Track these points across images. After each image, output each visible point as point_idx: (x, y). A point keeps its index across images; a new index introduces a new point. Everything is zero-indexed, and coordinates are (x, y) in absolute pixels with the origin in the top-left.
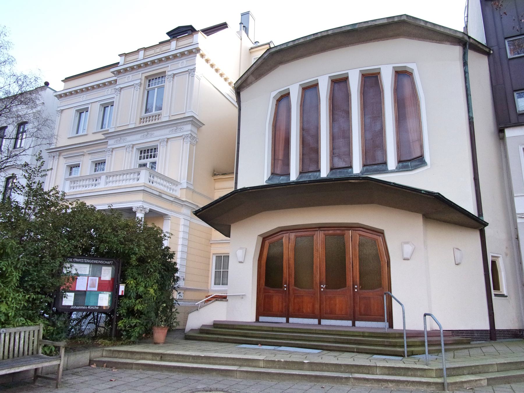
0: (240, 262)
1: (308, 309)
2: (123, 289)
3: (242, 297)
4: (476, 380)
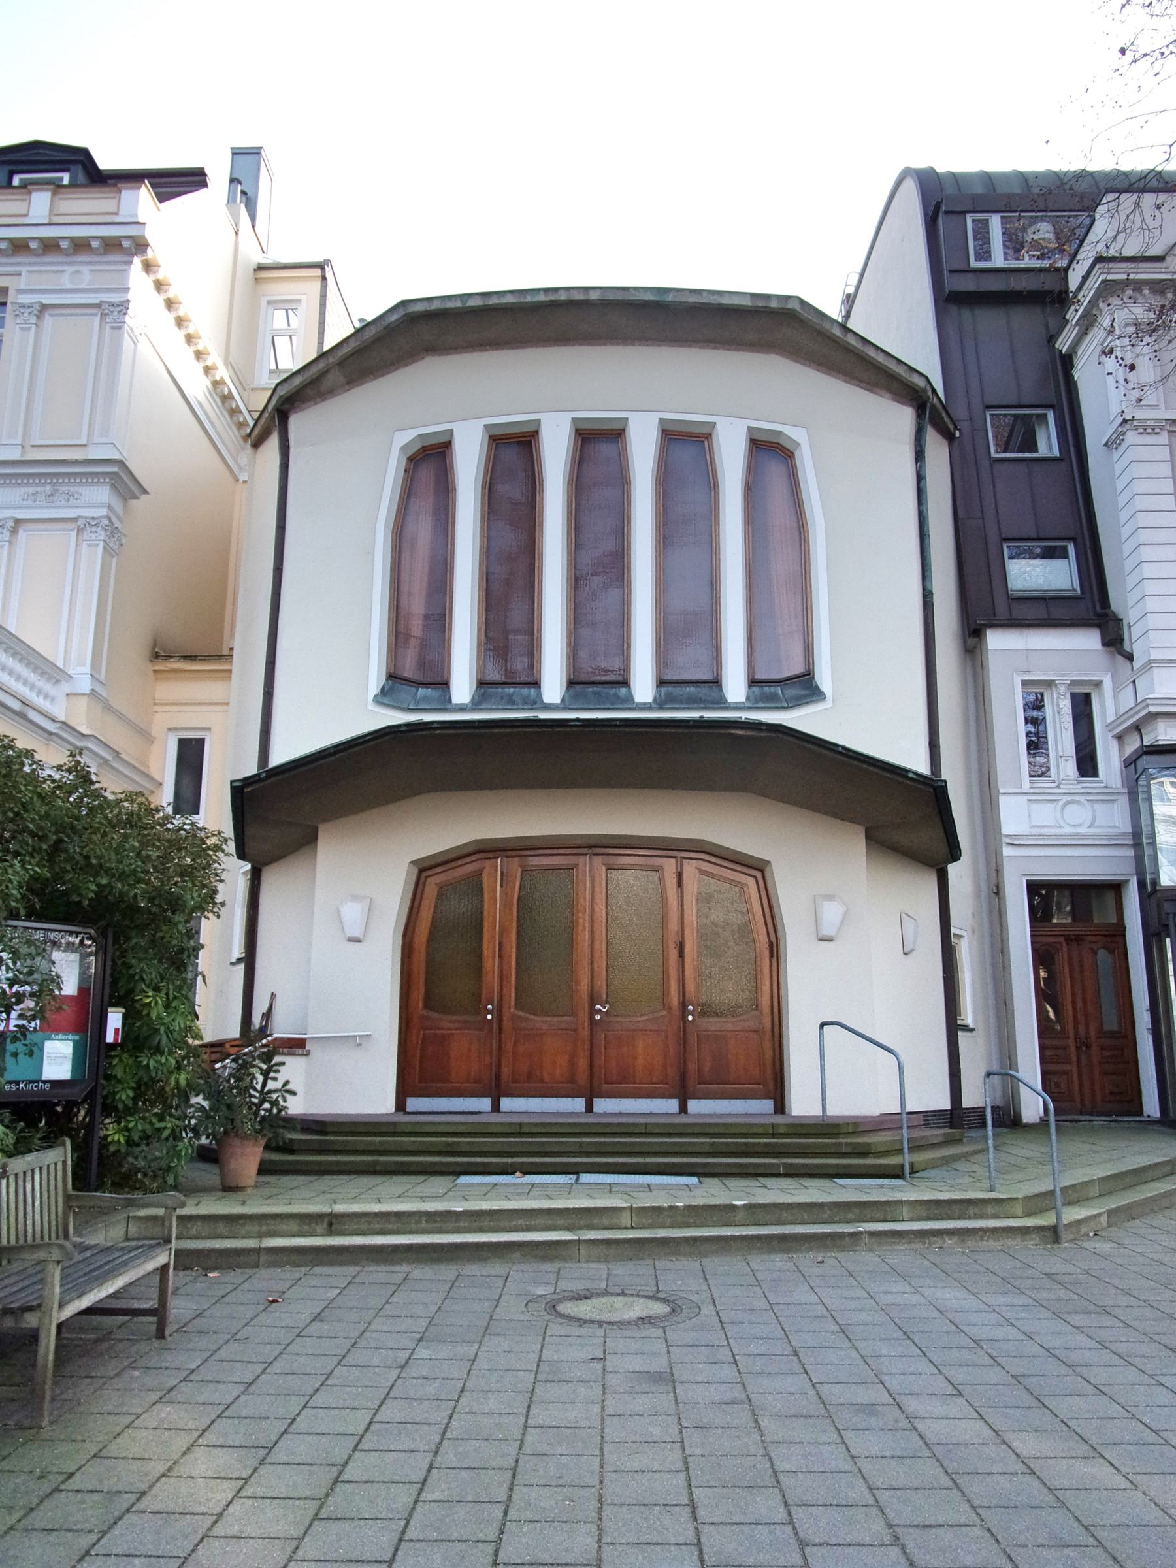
0: (352, 940)
1: (558, 1072)
2: (119, 1025)
3: (357, 1042)
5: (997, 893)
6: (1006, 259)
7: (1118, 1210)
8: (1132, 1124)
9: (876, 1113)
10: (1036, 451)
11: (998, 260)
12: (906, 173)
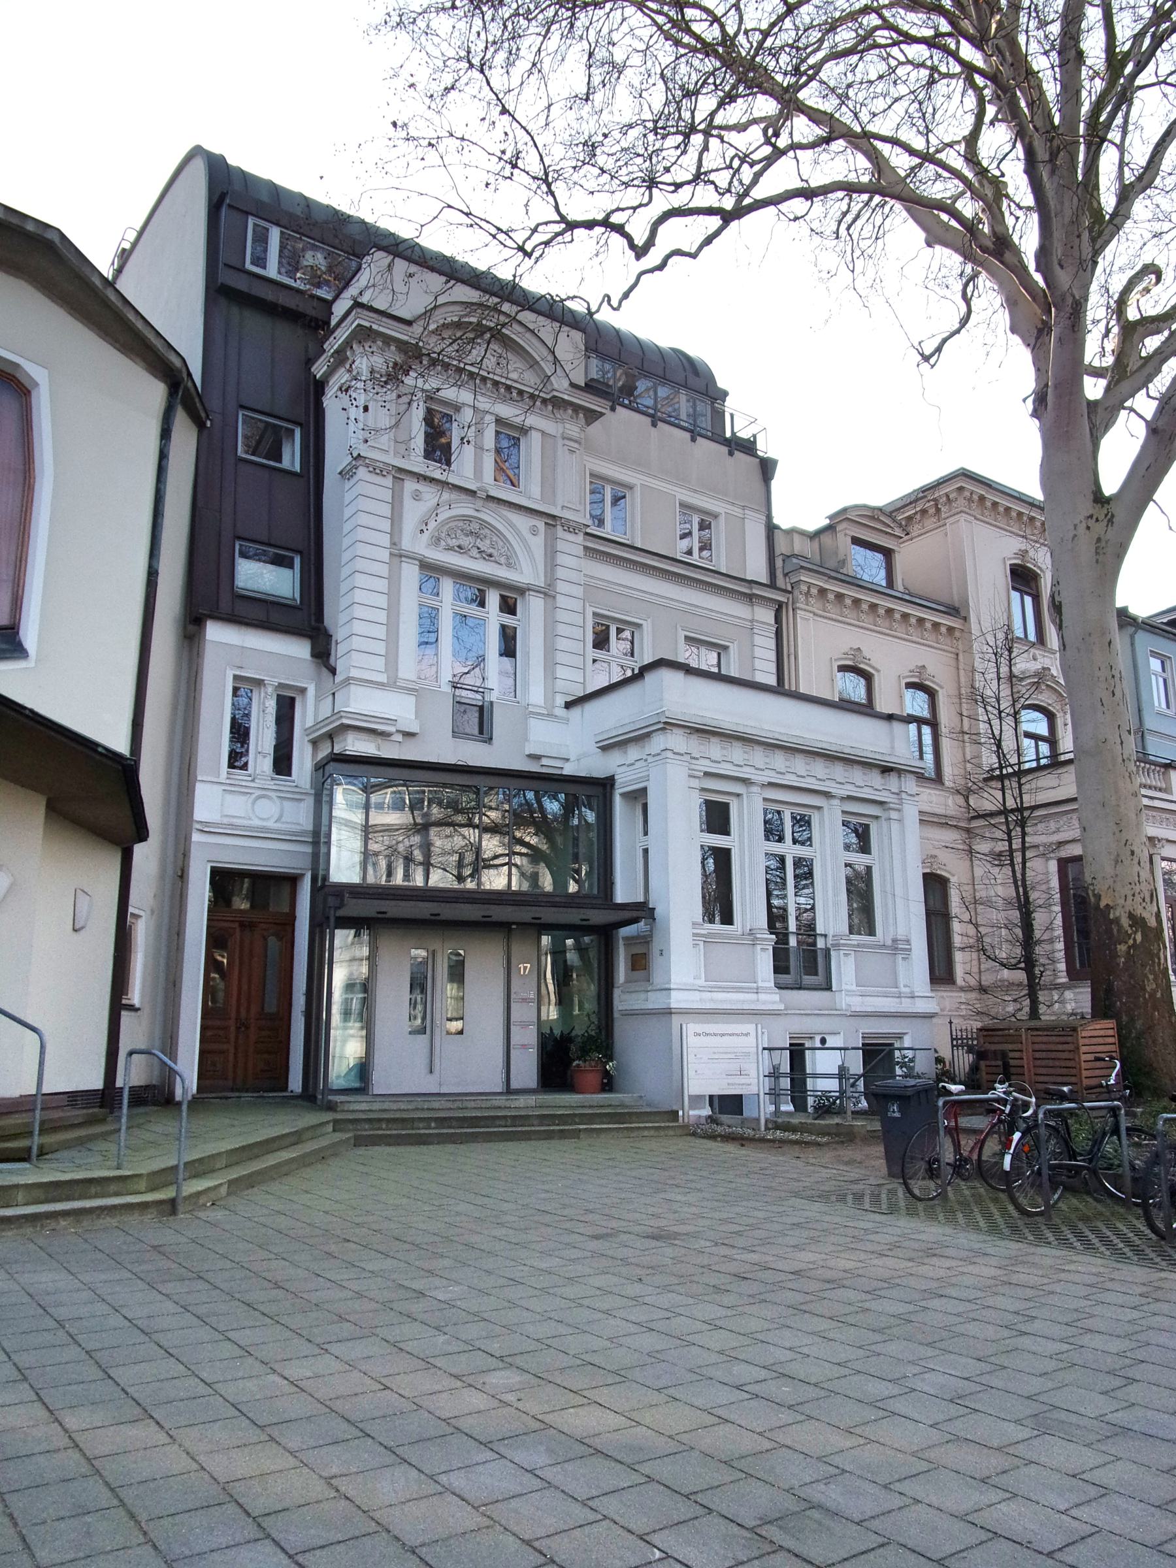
4: (209, 1189)
5: (181, 877)
6: (279, 273)
7: (236, 1180)
8: (278, 1100)
9: (17, 1095)
10: (280, 462)
11: (272, 270)
12: (197, 152)
